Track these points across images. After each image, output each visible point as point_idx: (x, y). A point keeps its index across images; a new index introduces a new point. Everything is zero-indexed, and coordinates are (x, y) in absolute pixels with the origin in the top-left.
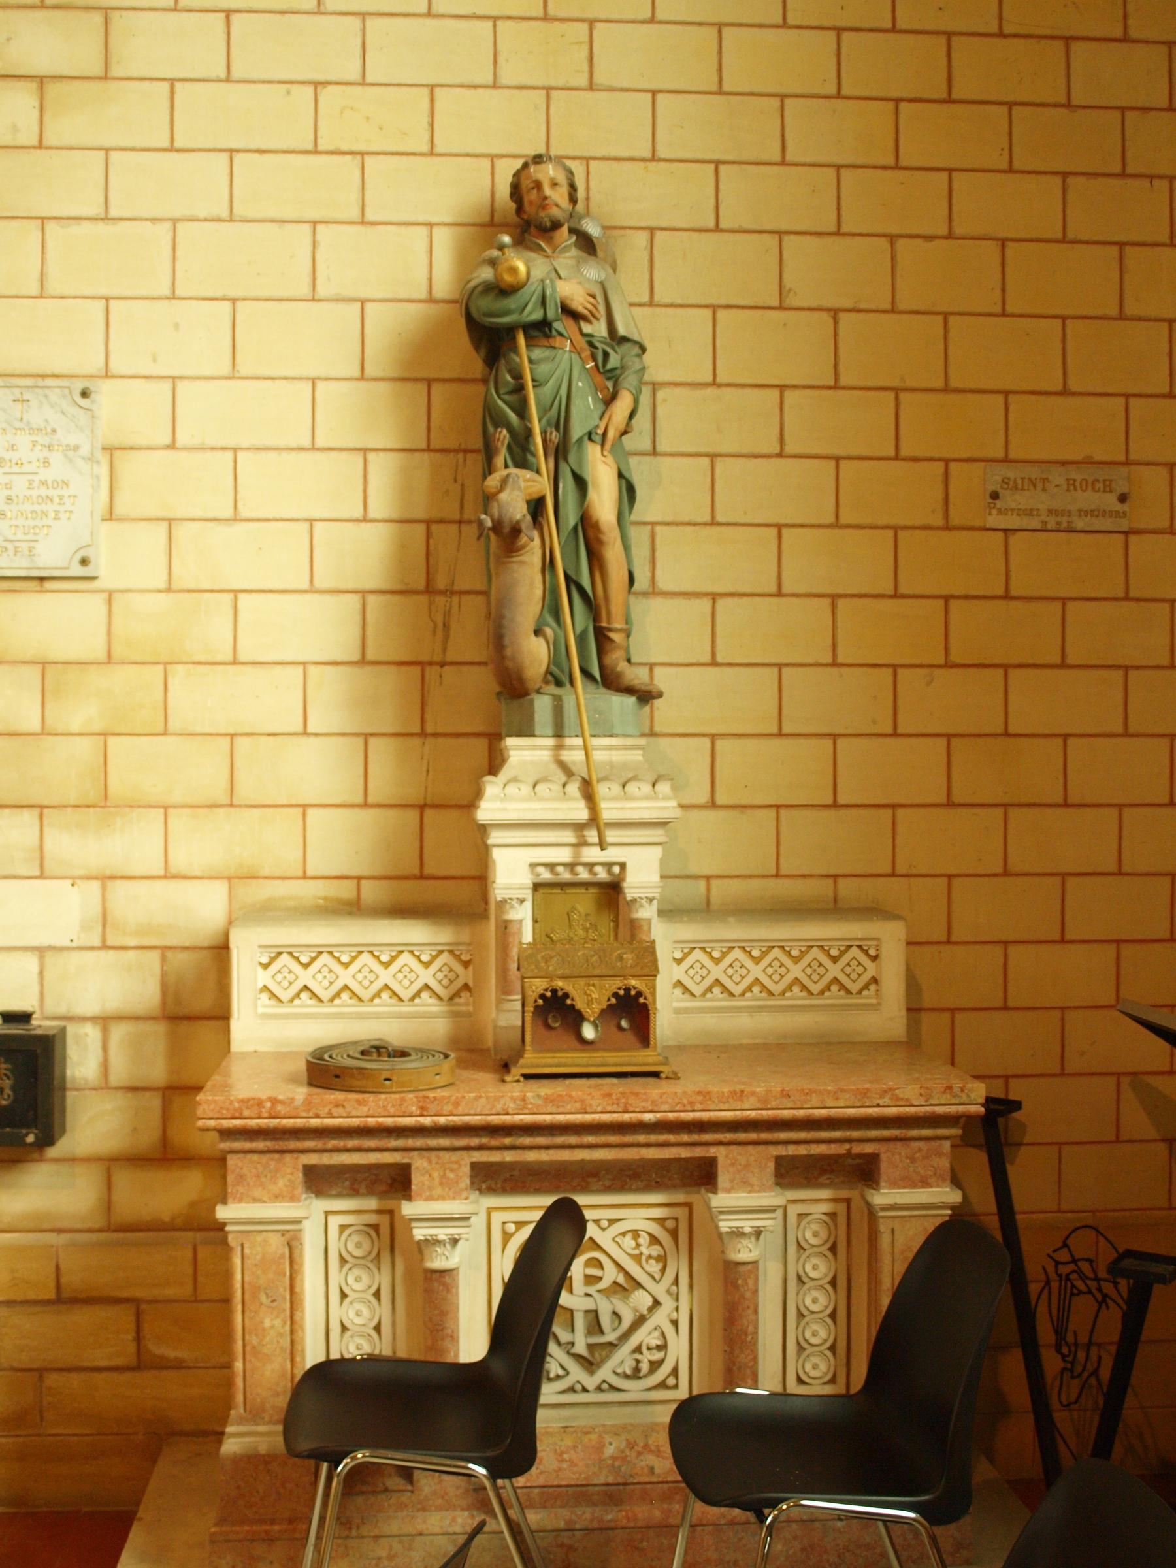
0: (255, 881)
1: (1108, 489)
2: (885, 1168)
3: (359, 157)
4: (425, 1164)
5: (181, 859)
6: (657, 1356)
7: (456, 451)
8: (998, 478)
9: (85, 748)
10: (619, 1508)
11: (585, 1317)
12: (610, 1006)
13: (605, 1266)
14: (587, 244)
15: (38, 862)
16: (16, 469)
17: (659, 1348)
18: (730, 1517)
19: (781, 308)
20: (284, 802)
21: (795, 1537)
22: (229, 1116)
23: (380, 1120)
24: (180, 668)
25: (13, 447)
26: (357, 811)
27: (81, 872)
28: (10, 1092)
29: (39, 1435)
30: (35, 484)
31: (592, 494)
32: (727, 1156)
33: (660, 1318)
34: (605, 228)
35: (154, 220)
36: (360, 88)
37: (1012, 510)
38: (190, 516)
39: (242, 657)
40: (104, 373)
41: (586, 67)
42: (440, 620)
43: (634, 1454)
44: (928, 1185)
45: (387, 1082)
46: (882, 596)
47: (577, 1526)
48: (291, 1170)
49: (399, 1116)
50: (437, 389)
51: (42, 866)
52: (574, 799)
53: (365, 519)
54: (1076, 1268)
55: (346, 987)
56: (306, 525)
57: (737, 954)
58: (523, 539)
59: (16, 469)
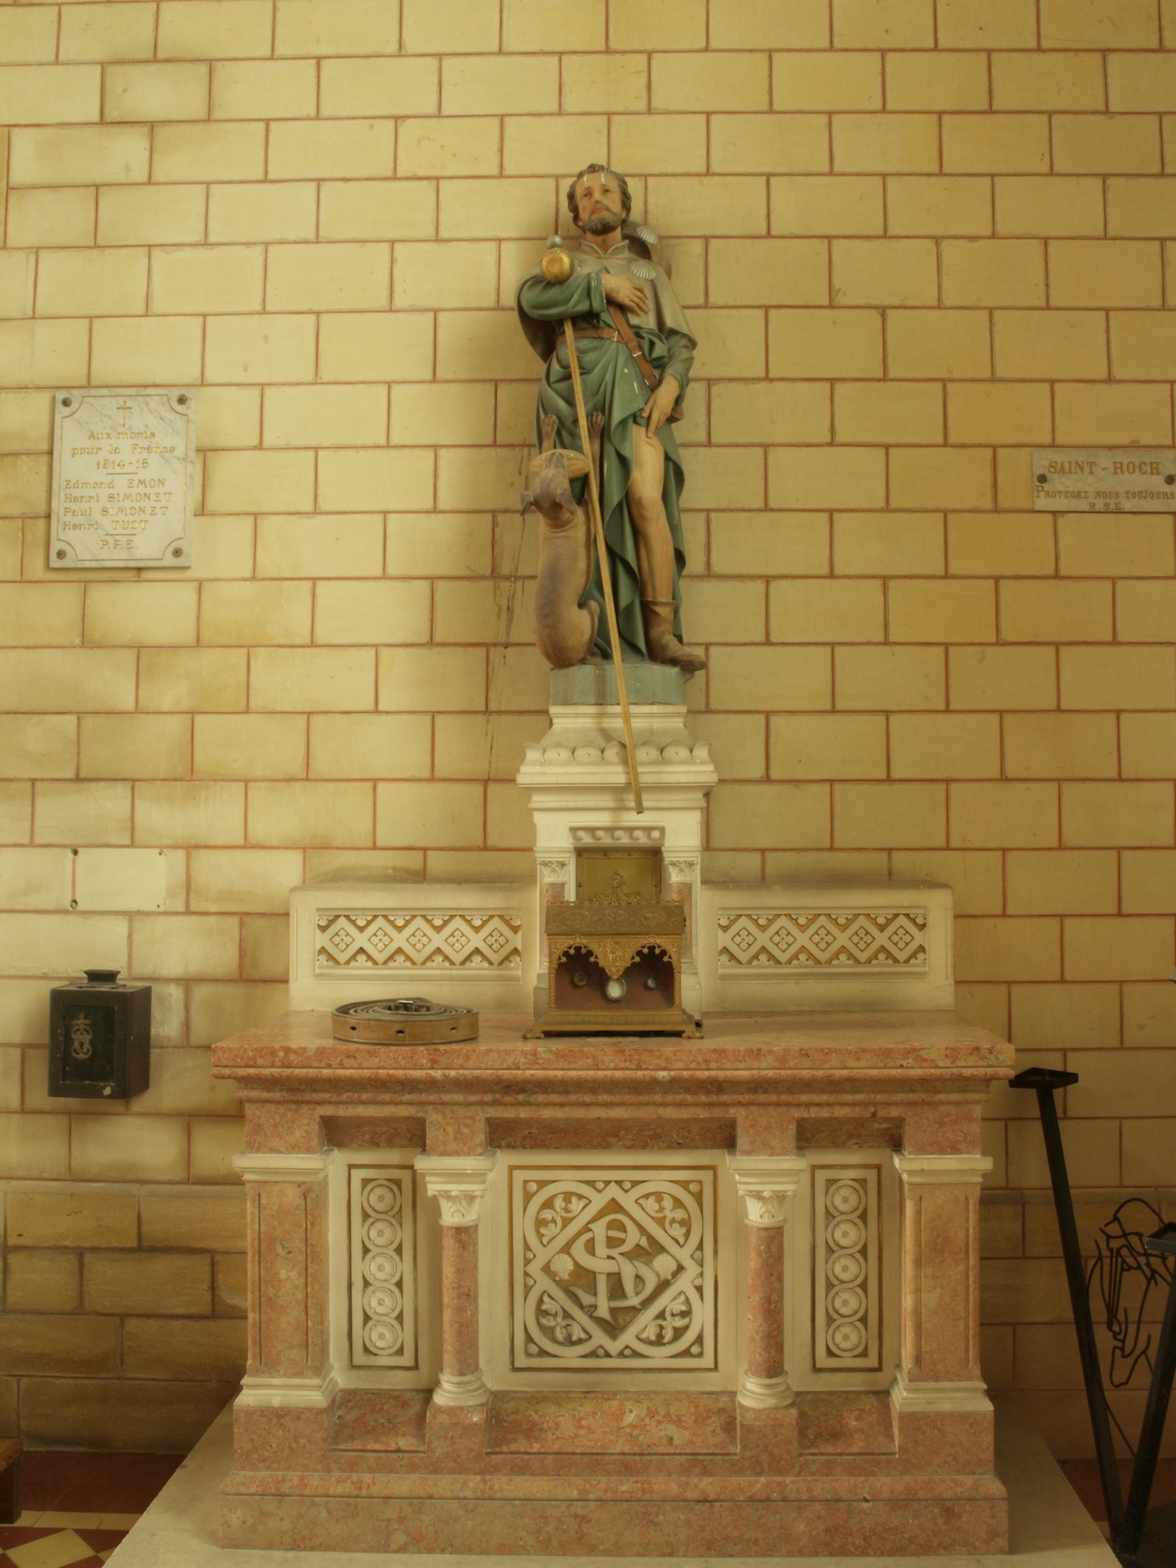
0: (328, 851)
1: (1155, 471)
2: (909, 1133)
3: (434, 182)
4: (440, 1118)
5: (260, 829)
6: (680, 1323)
7: (521, 446)
8: (1045, 463)
9: (173, 726)
10: (636, 1479)
11: (608, 1280)
12: (633, 964)
13: (628, 1228)
14: (641, 250)
15: (129, 832)
16: (118, 470)
17: (684, 1314)
18: (750, 1494)
19: (831, 306)
20: (357, 776)
21: (819, 1517)
22: (243, 1064)
23: (391, 1072)
24: (262, 650)
25: (116, 450)
26: (424, 785)
27: (168, 842)
28: (89, 1046)
29: (118, 1379)
30: (135, 483)
31: (636, 475)
32: (747, 1117)
33: (684, 1283)
34: (661, 238)
35: (248, 244)
36: (435, 121)
37: (1060, 492)
38: (275, 510)
39: (320, 639)
40: (200, 383)
41: (644, 93)
42: (504, 603)
43: (654, 1423)
44: (959, 1152)
45: (400, 1035)
46: (934, 577)
47: (591, 1496)
48: (307, 1123)
49: (410, 1069)
50: (503, 390)
51: (132, 835)
52: (613, 764)
53: (435, 511)
54: (1126, 1243)
55: (399, 951)
56: (380, 517)
57: (783, 921)
58: (566, 515)
59: (118, 470)
